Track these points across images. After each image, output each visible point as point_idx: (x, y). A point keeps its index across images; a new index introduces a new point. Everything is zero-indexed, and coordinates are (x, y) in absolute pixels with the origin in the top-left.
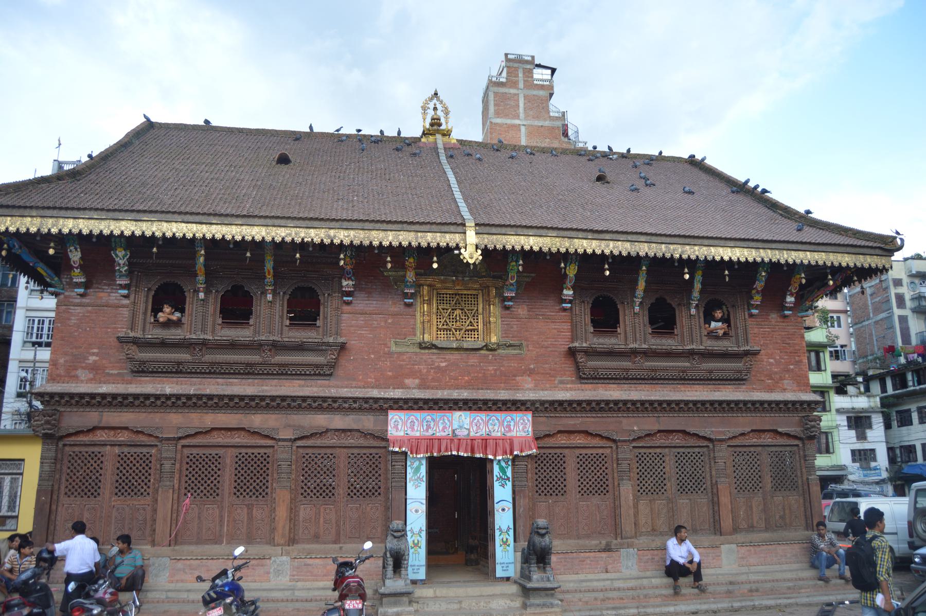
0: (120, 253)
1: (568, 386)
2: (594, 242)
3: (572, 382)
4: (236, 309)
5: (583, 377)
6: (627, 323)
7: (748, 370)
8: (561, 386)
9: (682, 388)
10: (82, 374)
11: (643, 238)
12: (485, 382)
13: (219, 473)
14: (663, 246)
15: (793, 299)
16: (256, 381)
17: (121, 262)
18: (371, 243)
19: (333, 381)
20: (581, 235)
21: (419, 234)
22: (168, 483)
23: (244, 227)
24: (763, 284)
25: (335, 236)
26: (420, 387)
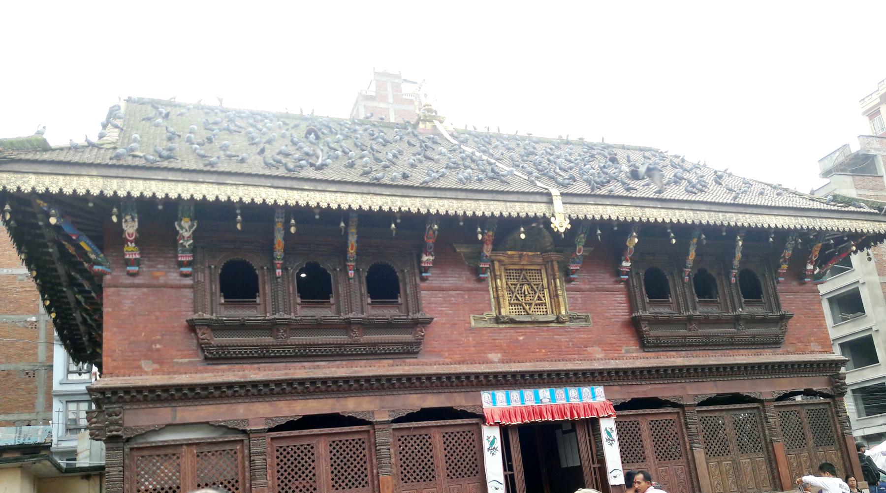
0: (186, 223)
1: (634, 355)
2: (663, 210)
3: (637, 351)
4: (316, 288)
5: (644, 344)
6: (408, 292)
7: (419, 343)
8: (629, 355)
9: (731, 352)
10: (146, 365)
11: (704, 207)
12: (560, 353)
13: (313, 465)
14: (720, 214)
15: (629, 264)
16: (344, 363)
17: (187, 234)
18: (465, 213)
19: (421, 359)
20: (651, 204)
21: (508, 204)
22: (262, 481)
23: (338, 195)
24: (790, 252)
25: (430, 205)
26: (503, 361)
